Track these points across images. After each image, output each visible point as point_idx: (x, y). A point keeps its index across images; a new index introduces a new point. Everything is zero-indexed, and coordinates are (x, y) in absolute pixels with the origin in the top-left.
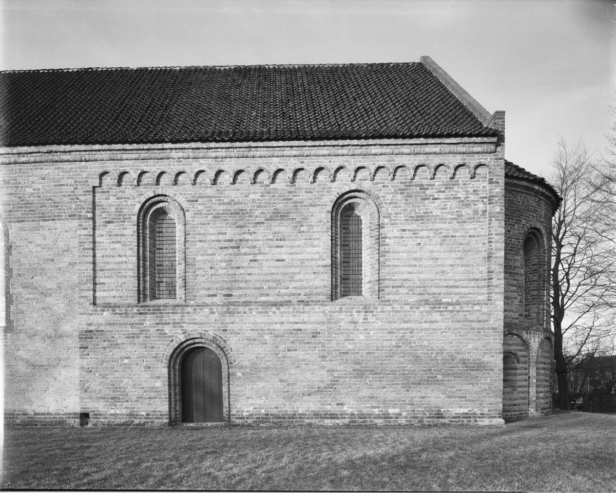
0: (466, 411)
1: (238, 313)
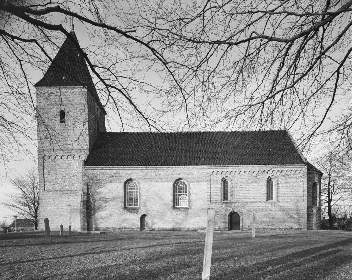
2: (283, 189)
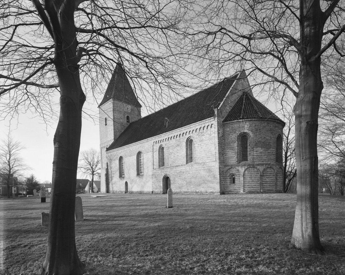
0: (212, 191)
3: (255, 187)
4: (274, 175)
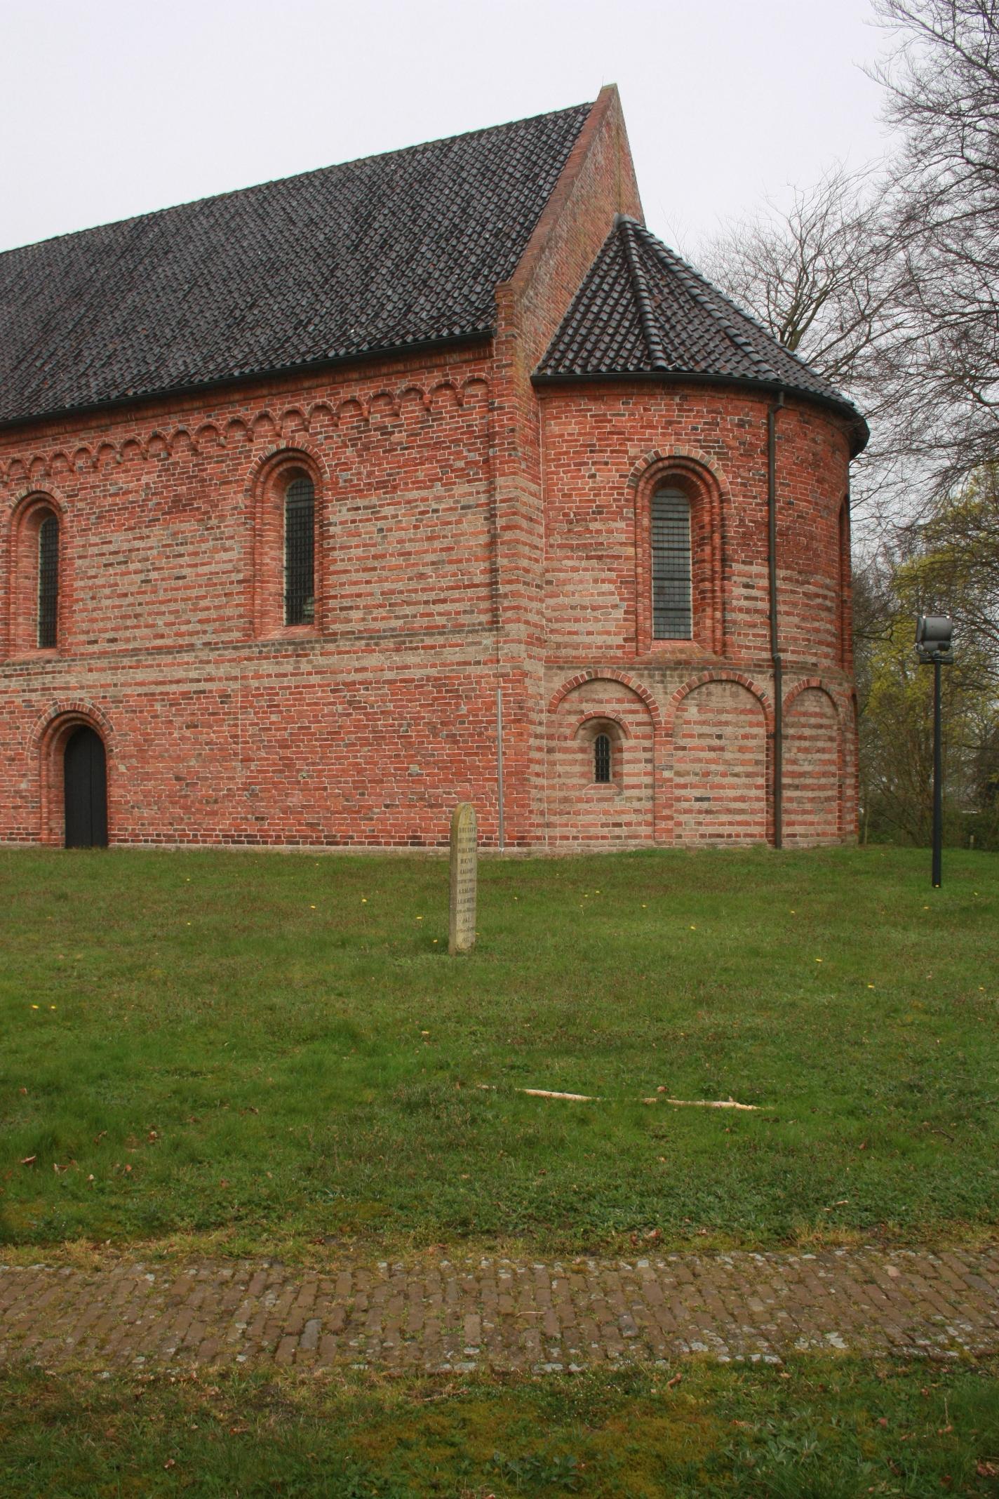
1: (124, 668)
2: (355, 541)
3: (742, 812)
4: (831, 739)
